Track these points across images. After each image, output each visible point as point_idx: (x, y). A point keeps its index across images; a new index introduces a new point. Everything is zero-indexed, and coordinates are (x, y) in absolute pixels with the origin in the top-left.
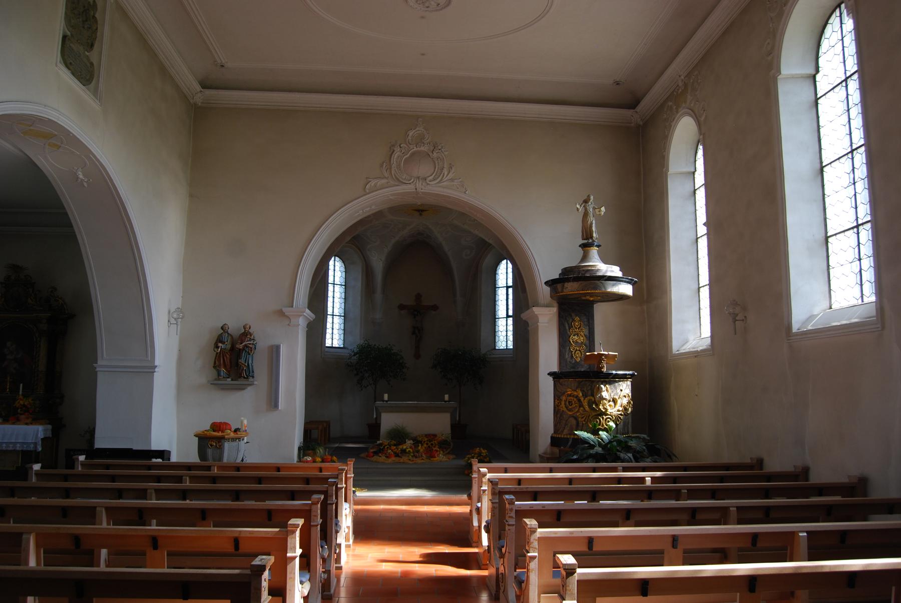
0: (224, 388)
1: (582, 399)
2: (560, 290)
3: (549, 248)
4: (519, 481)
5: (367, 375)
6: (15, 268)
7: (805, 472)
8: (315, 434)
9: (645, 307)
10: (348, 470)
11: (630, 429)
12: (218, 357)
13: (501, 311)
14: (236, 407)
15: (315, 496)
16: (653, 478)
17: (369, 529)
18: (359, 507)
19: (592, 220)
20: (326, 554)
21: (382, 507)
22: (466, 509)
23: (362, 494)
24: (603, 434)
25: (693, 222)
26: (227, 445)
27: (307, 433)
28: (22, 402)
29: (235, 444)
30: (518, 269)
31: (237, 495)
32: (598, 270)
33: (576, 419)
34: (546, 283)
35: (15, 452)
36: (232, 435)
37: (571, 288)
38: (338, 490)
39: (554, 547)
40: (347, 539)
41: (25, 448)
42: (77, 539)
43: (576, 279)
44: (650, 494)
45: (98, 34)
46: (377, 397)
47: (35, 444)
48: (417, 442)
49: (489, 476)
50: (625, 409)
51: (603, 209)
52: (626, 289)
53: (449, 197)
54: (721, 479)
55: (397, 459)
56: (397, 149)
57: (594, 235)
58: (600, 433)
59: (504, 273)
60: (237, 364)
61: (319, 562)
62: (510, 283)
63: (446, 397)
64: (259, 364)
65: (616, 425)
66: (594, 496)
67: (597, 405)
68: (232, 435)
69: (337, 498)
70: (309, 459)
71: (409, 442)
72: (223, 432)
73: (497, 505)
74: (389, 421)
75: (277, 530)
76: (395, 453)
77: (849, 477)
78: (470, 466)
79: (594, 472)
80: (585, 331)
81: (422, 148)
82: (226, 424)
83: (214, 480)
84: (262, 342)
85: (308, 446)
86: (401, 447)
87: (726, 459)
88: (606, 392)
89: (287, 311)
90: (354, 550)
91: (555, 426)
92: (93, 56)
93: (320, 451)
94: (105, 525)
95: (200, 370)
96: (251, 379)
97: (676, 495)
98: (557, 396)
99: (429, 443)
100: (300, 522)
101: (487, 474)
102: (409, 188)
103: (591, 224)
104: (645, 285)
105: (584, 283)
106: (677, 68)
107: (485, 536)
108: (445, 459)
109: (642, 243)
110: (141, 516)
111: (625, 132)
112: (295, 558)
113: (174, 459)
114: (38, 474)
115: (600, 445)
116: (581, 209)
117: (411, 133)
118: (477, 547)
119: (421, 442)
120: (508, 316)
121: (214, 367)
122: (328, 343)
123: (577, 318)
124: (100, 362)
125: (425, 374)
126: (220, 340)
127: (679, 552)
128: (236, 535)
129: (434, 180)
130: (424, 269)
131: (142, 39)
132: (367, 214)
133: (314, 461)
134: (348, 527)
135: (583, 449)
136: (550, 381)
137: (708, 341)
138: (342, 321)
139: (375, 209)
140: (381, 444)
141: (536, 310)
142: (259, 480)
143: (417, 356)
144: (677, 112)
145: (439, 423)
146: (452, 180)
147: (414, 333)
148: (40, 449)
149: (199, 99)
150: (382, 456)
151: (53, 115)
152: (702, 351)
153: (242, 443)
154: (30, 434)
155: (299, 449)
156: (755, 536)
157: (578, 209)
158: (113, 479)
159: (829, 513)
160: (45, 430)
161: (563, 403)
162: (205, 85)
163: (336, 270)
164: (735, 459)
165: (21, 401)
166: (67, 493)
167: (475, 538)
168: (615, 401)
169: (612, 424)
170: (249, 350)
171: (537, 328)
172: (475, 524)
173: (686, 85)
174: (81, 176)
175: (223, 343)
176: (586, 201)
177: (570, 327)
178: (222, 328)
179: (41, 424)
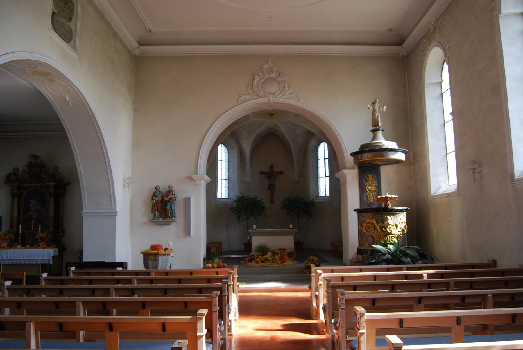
1: (376, 225)
2: (360, 158)
3: (352, 134)
4: (342, 278)
5: (242, 214)
6: (34, 157)
7: (494, 263)
8: (213, 250)
9: (412, 168)
10: (235, 273)
11: (406, 243)
12: (154, 205)
14: (166, 235)
15: (215, 292)
16: (428, 274)
17: (248, 309)
18: (241, 294)
19: (378, 114)
20: (222, 329)
21: (255, 294)
22: (308, 294)
23: (243, 286)
24: (391, 247)
25: (442, 113)
26: (160, 258)
27: (208, 249)
28: (40, 236)
29: (165, 257)
31: (165, 292)
32: (383, 145)
33: (372, 237)
34: (351, 154)
35: (37, 264)
36: (163, 252)
37: (367, 157)
38: (228, 286)
39: (381, 332)
40: (235, 316)
41: (43, 262)
42: (61, 326)
43: (370, 151)
44: (429, 286)
45: (75, 12)
46: (249, 227)
48: (274, 253)
49: (323, 275)
50: (403, 231)
51: (385, 107)
52: (401, 156)
53: (289, 104)
54: (472, 275)
55: (262, 264)
56: (257, 77)
57: (380, 124)
58: (389, 245)
59: (323, 150)
60: (165, 210)
61: (218, 334)
62: (327, 157)
63: (291, 226)
64: (178, 208)
65: (398, 240)
66: (393, 288)
67: (386, 229)
68: (163, 252)
69: (228, 292)
70: (210, 265)
71: (269, 254)
72: (158, 250)
73: (330, 295)
74: (257, 241)
75: (190, 317)
76: (261, 260)
77: (520, 265)
78: (310, 268)
79: (388, 271)
80: (376, 183)
81: (272, 75)
82: (159, 245)
83: (152, 281)
85: (209, 257)
86: (264, 257)
87: (470, 260)
88: (391, 220)
89: (193, 176)
90: (239, 322)
91: (359, 242)
92: (72, 25)
93: (217, 260)
94: (82, 315)
95: (143, 213)
96: (174, 218)
97: (447, 286)
98: (360, 224)
99: (281, 254)
100: (205, 312)
101: (322, 274)
102: (265, 100)
103: (378, 117)
104: (411, 154)
105: (375, 153)
106: (429, 18)
107: (321, 313)
109: (409, 126)
110: (104, 309)
111: (398, 61)
112: (202, 336)
113: (130, 268)
114: (45, 279)
115: (389, 253)
116: (371, 108)
117: (265, 67)
118: (316, 319)
119: (276, 253)
120: (326, 176)
121: (152, 212)
122: (219, 196)
123: (370, 176)
124: (84, 210)
125: (277, 213)
126: (154, 195)
127: (461, 328)
128: (164, 321)
129: (280, 94)
130: (274, 149)
131: (101, 16)
132: (241, 117)
133: (213, 267)
134: (235, 308)
135: (379, 256)
136: (355, 214)
137: (456, 187)
138: (227, 182)
139: (244, 113)
140: (253, 255)
141: (345, 171)
142: (180, 281)
143: (272, 202)
144: (430, 45)
145: (287, 242)
146: (291, 94)
147: (269, 188)
148: (51, 263)
149: (137, 52)
150: (251, 261)
151: (48, 61)
152: (451, 193)
153: (169, 257)
154: (46, 254)
155: (204, 259)
156: (514, 317)
157: (369, 108)
158: (90, 282)
159: (506, 284)
160: (54, 252)
161: (364, 228)
162: (141, 44)
163: (222, 152)
164: (476, 261)
165: (40, 235)
166: (61, 292)
167: (315, 314)
168: (396, 226)
169: (395, 240)
170: (172, 201)
171: (345, 183)
172: (314, 304)
173: (435, 28)
174: (68, 99)
175: (156, 197)
176: (374, 103)
177: (366, 181)
178: (156, 188)
179: (52, 248)
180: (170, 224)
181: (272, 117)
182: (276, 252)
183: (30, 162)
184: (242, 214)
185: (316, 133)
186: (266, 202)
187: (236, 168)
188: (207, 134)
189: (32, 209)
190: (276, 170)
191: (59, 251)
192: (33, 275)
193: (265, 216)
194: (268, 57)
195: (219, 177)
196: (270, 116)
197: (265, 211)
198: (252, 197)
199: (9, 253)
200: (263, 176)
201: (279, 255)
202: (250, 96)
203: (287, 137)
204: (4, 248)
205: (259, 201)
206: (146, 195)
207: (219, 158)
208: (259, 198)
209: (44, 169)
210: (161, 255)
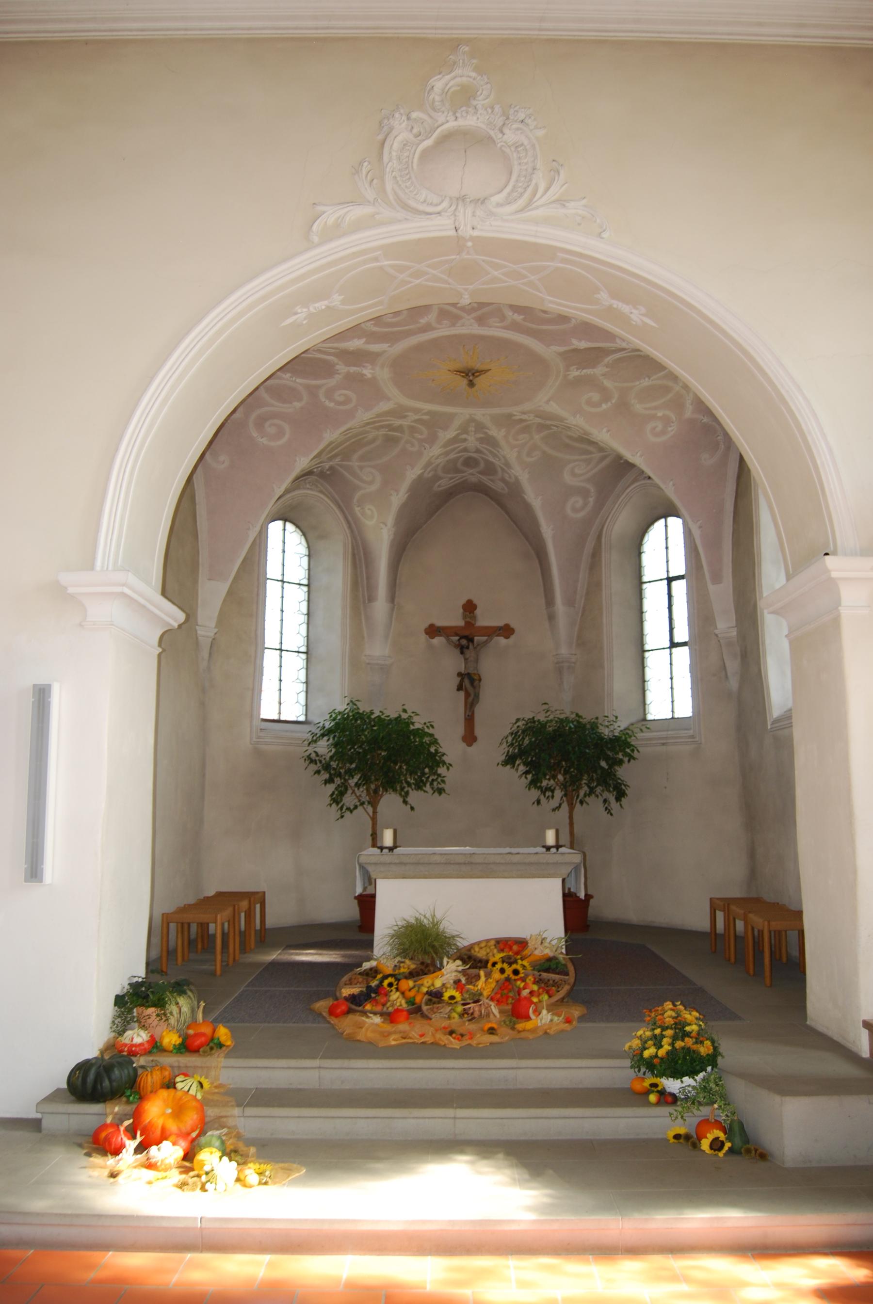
13: (655, 632)
30: (690, 531)
48: (473, 961)
62: (679, 567)
71: (451, 969)
74: (399, 903)
76: (411, 1002)
120: (673, 645)
122: (268, 711)
129: (508, 202)
140: (374, 972)
143: (470, 738)
146: (561, 202)
147: (460, 688)
182: (481, 954)
187: (339, 613)
188: (152, 379)
190: (484, 620)
193: (440, 791)
194: (454, 44)
195: (271, 638)
197: (442, 770)
198: (393, 715)
200: (438, 641)
201: (497, 975)
202: (367, 210)
208: (418, 723)
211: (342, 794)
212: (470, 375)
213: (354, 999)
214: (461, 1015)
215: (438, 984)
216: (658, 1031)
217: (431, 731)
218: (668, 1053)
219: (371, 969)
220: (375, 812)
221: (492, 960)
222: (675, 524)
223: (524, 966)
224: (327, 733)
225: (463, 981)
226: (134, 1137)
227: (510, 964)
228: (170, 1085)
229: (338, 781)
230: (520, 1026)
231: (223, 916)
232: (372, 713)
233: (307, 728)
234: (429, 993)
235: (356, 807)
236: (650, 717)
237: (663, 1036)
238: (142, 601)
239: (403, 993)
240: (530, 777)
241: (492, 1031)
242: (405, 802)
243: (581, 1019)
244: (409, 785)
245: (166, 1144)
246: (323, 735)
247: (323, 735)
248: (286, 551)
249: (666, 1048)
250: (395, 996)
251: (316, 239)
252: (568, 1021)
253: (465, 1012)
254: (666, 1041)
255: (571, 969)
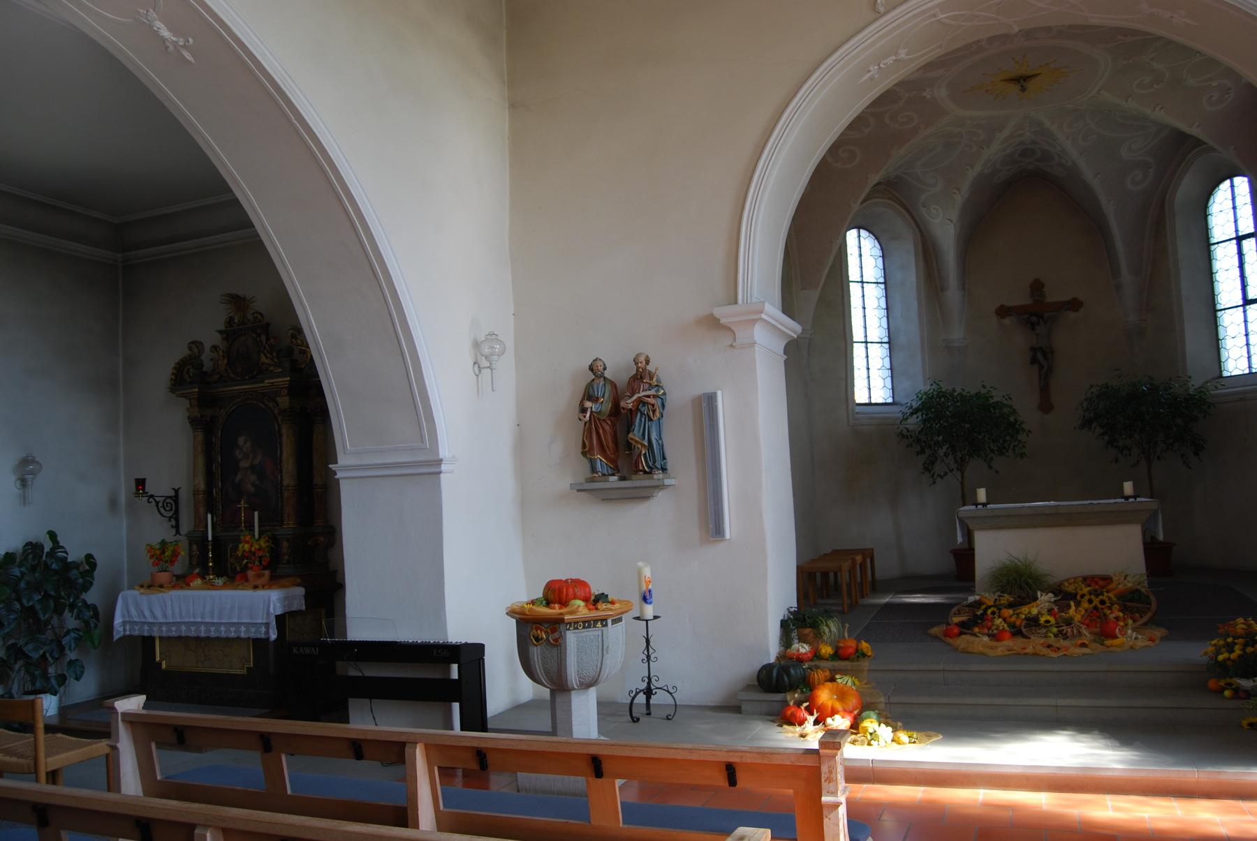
0: (609, 497)
41: (253, 634)
47: (267, 625)
48: (1064, 596)
55: (1015, 644)
60: (629, 446)
63: (1128, 487)
64: (676, 439)
71: (1045, 599)
74: (993, 549)
76: (1012, 626)
84: (679, 393)
86: (1025, 609)
89: (724, 313)
95: (558, 460)
96: (658, 475)
99: (1096, 603)
108: (1142, 642)
119: (1073, 596)
121: (584, 454)
122: (860, 396)
124: (343, 460)
126: (589, 395)
140: (978, 604)
143: (1046, 406)
145: (1115, 550)
147: (1034, 361)
155: (784, 624)
178: (591, 368)
180: (647, 498)
181: (1023, 89)
182: (1071, 589)
183: (230, 321)
184: (941, 452)
185: (1202, 136)
186: (1026, 408)
187: (915, 304)
189: (243, 464)
190: (1054, 295)
191: (307, 596)
192: (233, 672)
193: (1022, 455)
195: (858, 334)
196: (1015, 88)
197: (1021, 437)
198: (973, 392)
199: (169, 603)
201: (1086, 605)
203: (1088, 174)
204: (161, 586)
205: (998, 405)
206: (565, 395)
207: (853, 274)
208: (997, 397)
209: (263, 338)
210: (575, 624)
211: (933, 463)
212: (1021, 81)
213: (962, 625)
214: (1056, 636)
215: (1035, 611)
216: (1230, 640)
217: (1009, 403)
218: (1239, 656)
219: (975, 602)
220: (962, 477)
221: (1080, 593)
222: (1242, 183)
223: (1109, 598)
224: (916, 411)
225: (1056, 609)
226: (812, 714)
227: (1097, 596)
228: (833, 680)
229: (928, 452)
230: (1108, 642)
231: (846, 565)
232: (954, 390)
233: (896, 409)
234: (1027, 619)
235: (946, 474)
236: (1225, 374)
237: (1235, 644)
238: (773, 322)
239: (1004, 620)
240: (1106, 438)
241: (1083, 645)
242: (990, 467)
243: (1163, 639)
244: (992, 451)
245: (837, 717)
246: (912, 414)
247: (912, 414)
248: (863, 254)
249: (1238, 651)
250: (998, 621)
251: (882, 9)
252: (1151, 640)
253: (1060, 632)
254: (1237, 647)
255: (1153, 599)
